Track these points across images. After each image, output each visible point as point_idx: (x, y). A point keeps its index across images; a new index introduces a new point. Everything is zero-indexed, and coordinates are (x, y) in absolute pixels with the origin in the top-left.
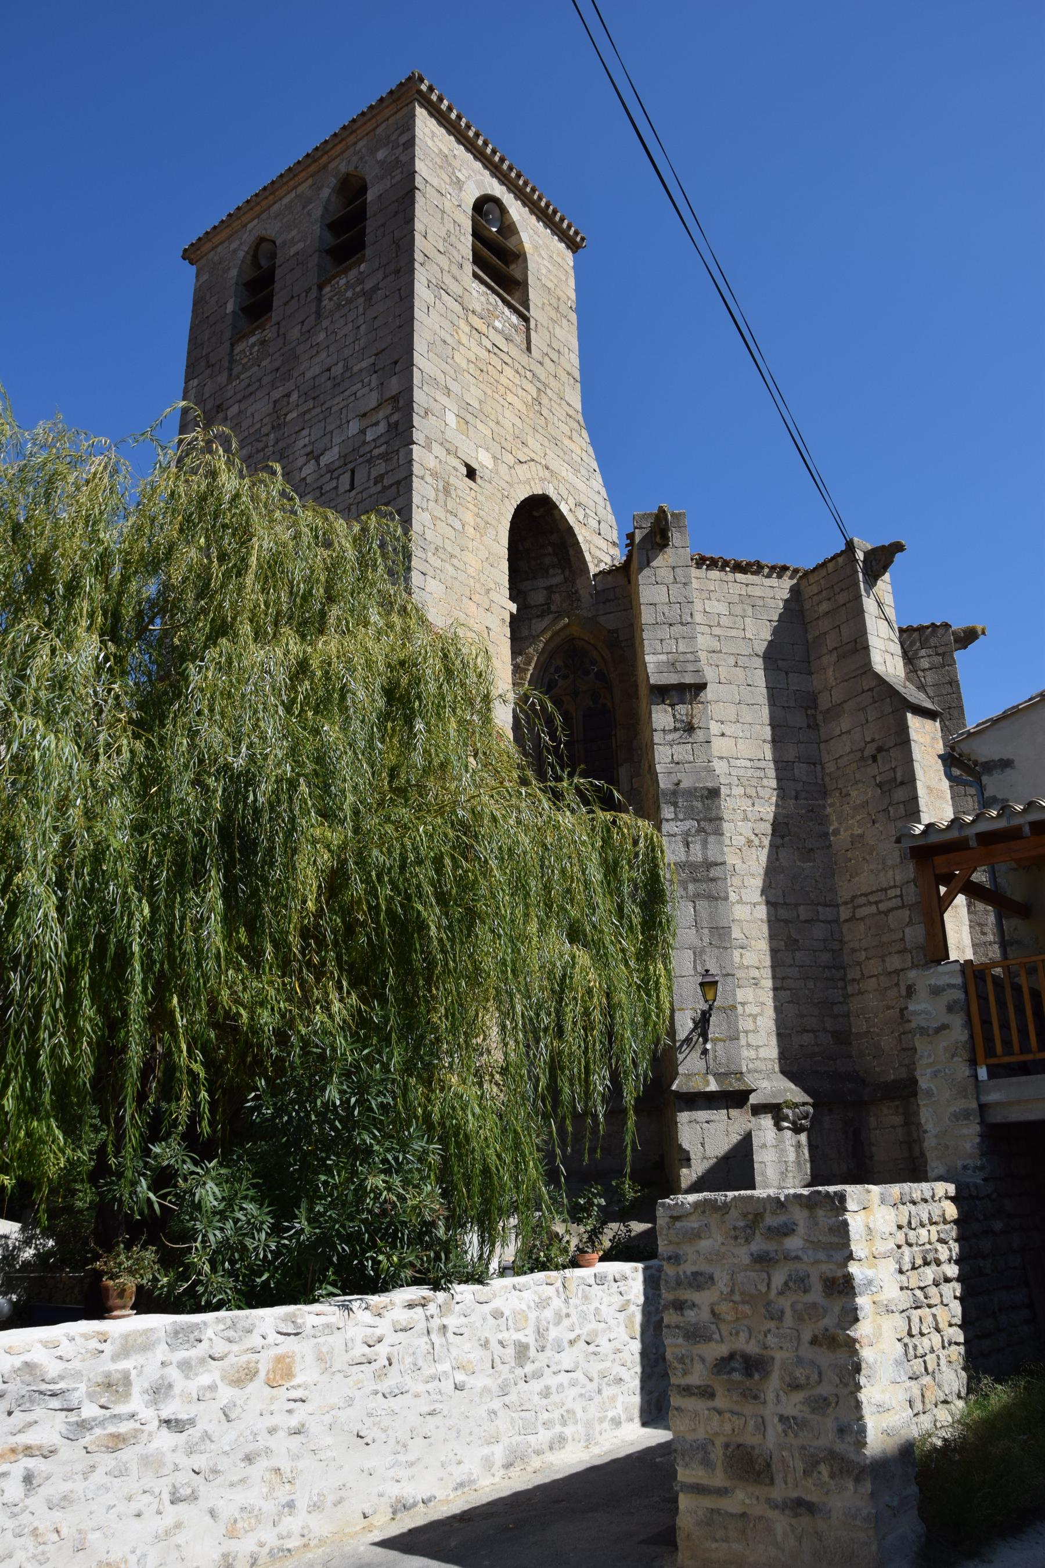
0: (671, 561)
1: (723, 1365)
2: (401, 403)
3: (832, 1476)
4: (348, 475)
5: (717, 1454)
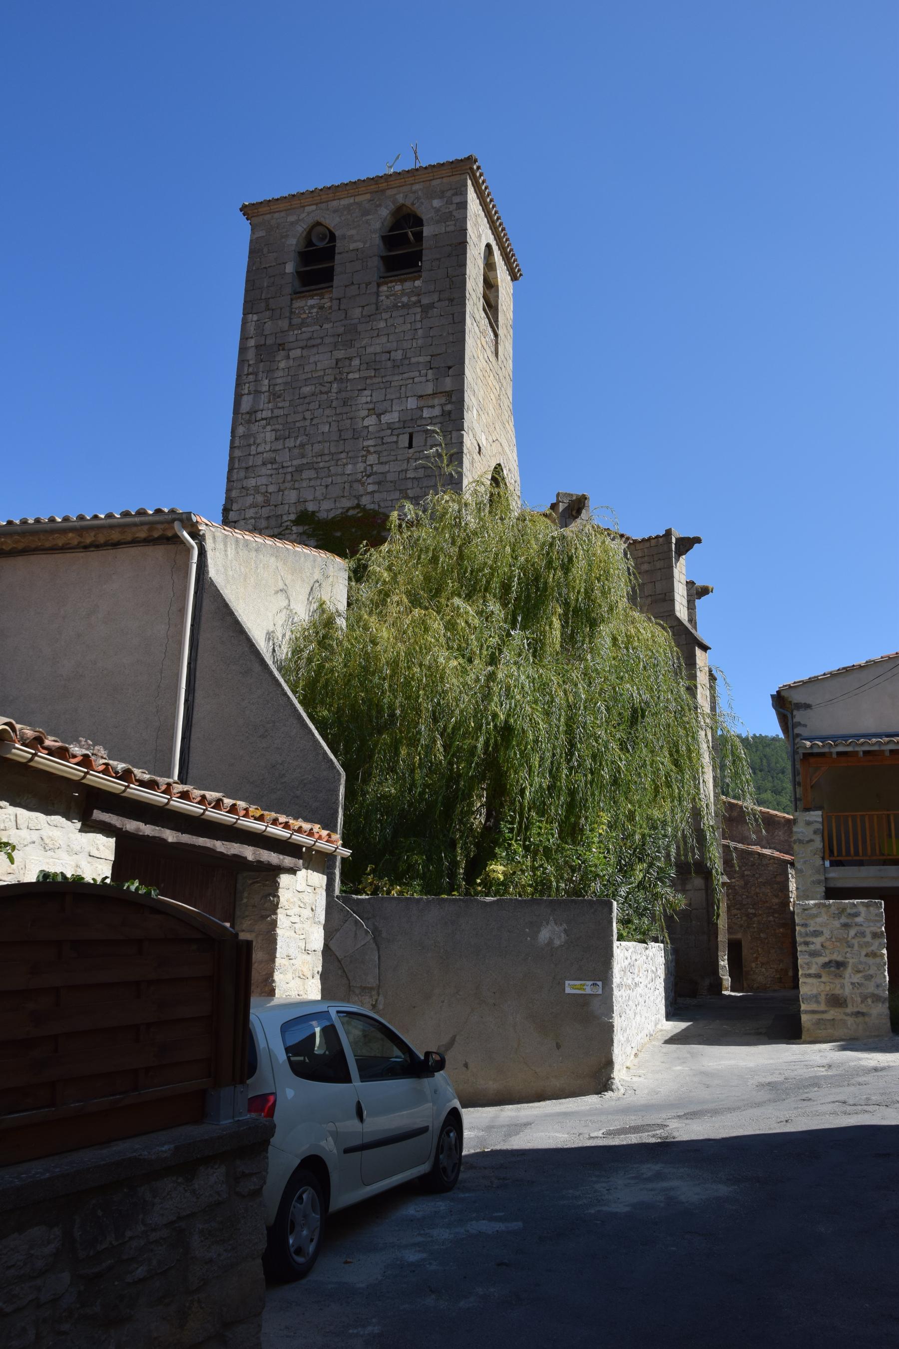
1: (826, 965)
2: (454, 399)
3: (873, 1002)
4: (407, 437)
5: (822, 998)
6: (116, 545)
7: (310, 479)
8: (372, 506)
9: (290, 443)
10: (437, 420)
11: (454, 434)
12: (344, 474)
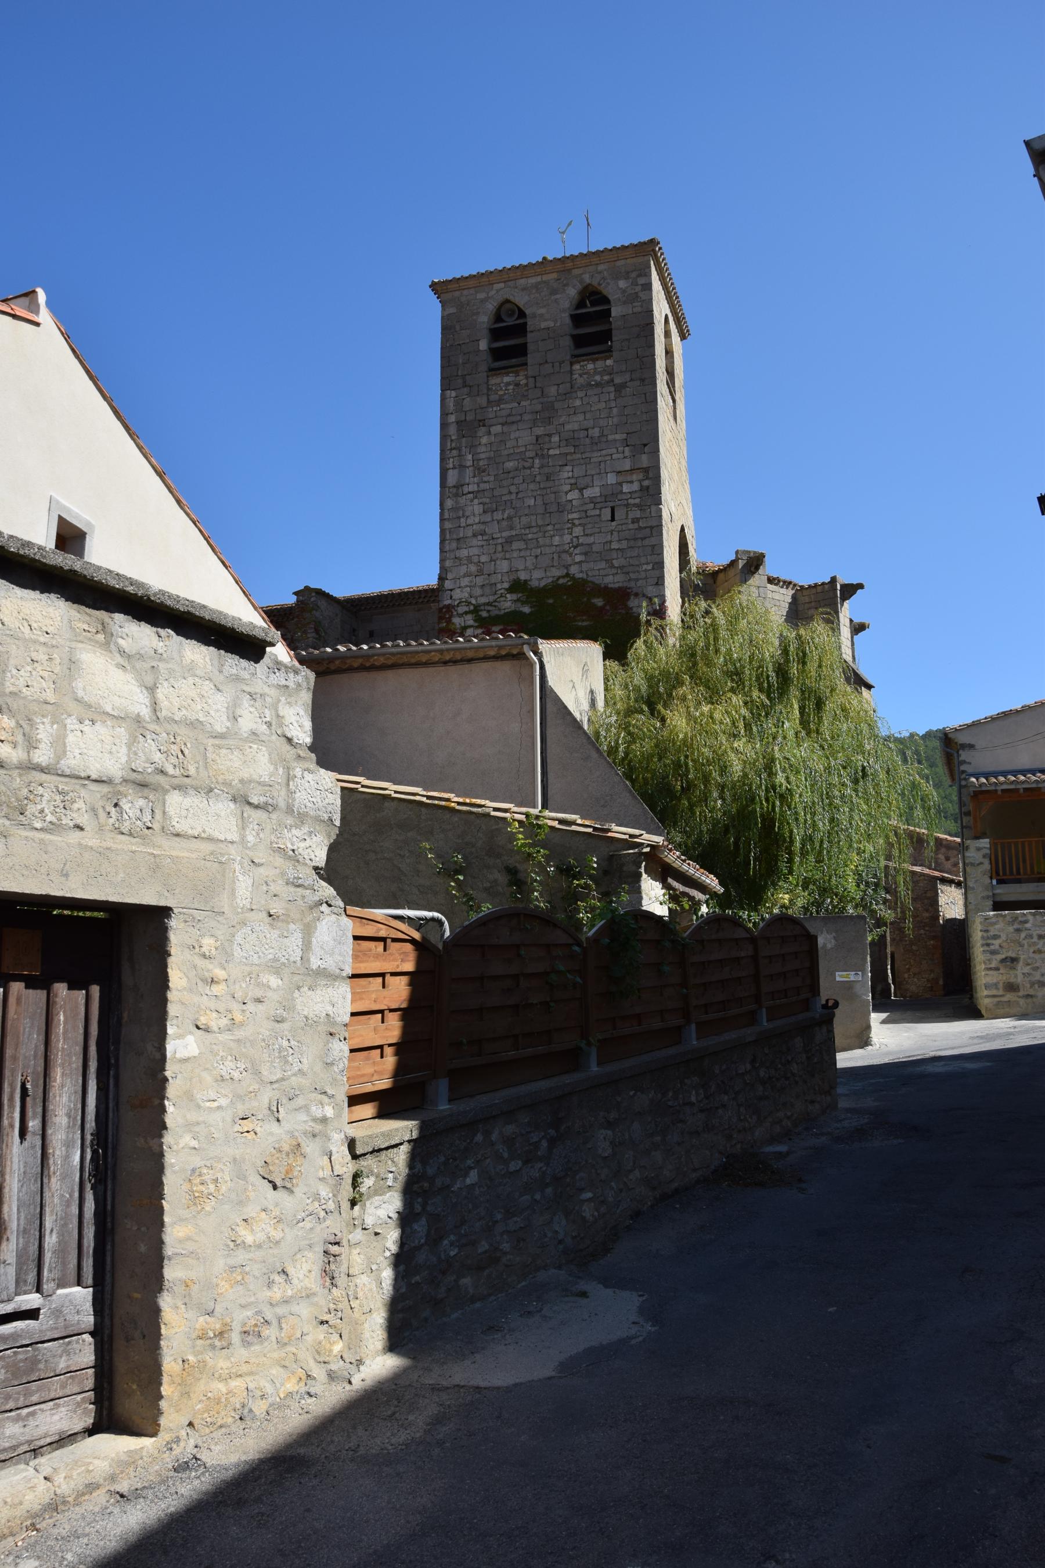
0: (757, 583)
1: (1003, 961)
2: (651, 475)
4: (609, 510)
5: (1001, 985)
6: (470, 661)
7: (520, 550)
8: (581, 575)
9: (498, 516)
10: (637, 495)
11: (653, 508)
12: (552, 545)
